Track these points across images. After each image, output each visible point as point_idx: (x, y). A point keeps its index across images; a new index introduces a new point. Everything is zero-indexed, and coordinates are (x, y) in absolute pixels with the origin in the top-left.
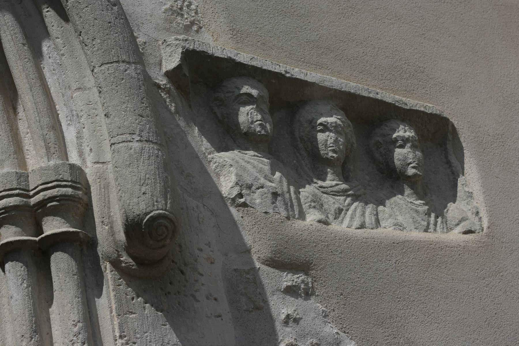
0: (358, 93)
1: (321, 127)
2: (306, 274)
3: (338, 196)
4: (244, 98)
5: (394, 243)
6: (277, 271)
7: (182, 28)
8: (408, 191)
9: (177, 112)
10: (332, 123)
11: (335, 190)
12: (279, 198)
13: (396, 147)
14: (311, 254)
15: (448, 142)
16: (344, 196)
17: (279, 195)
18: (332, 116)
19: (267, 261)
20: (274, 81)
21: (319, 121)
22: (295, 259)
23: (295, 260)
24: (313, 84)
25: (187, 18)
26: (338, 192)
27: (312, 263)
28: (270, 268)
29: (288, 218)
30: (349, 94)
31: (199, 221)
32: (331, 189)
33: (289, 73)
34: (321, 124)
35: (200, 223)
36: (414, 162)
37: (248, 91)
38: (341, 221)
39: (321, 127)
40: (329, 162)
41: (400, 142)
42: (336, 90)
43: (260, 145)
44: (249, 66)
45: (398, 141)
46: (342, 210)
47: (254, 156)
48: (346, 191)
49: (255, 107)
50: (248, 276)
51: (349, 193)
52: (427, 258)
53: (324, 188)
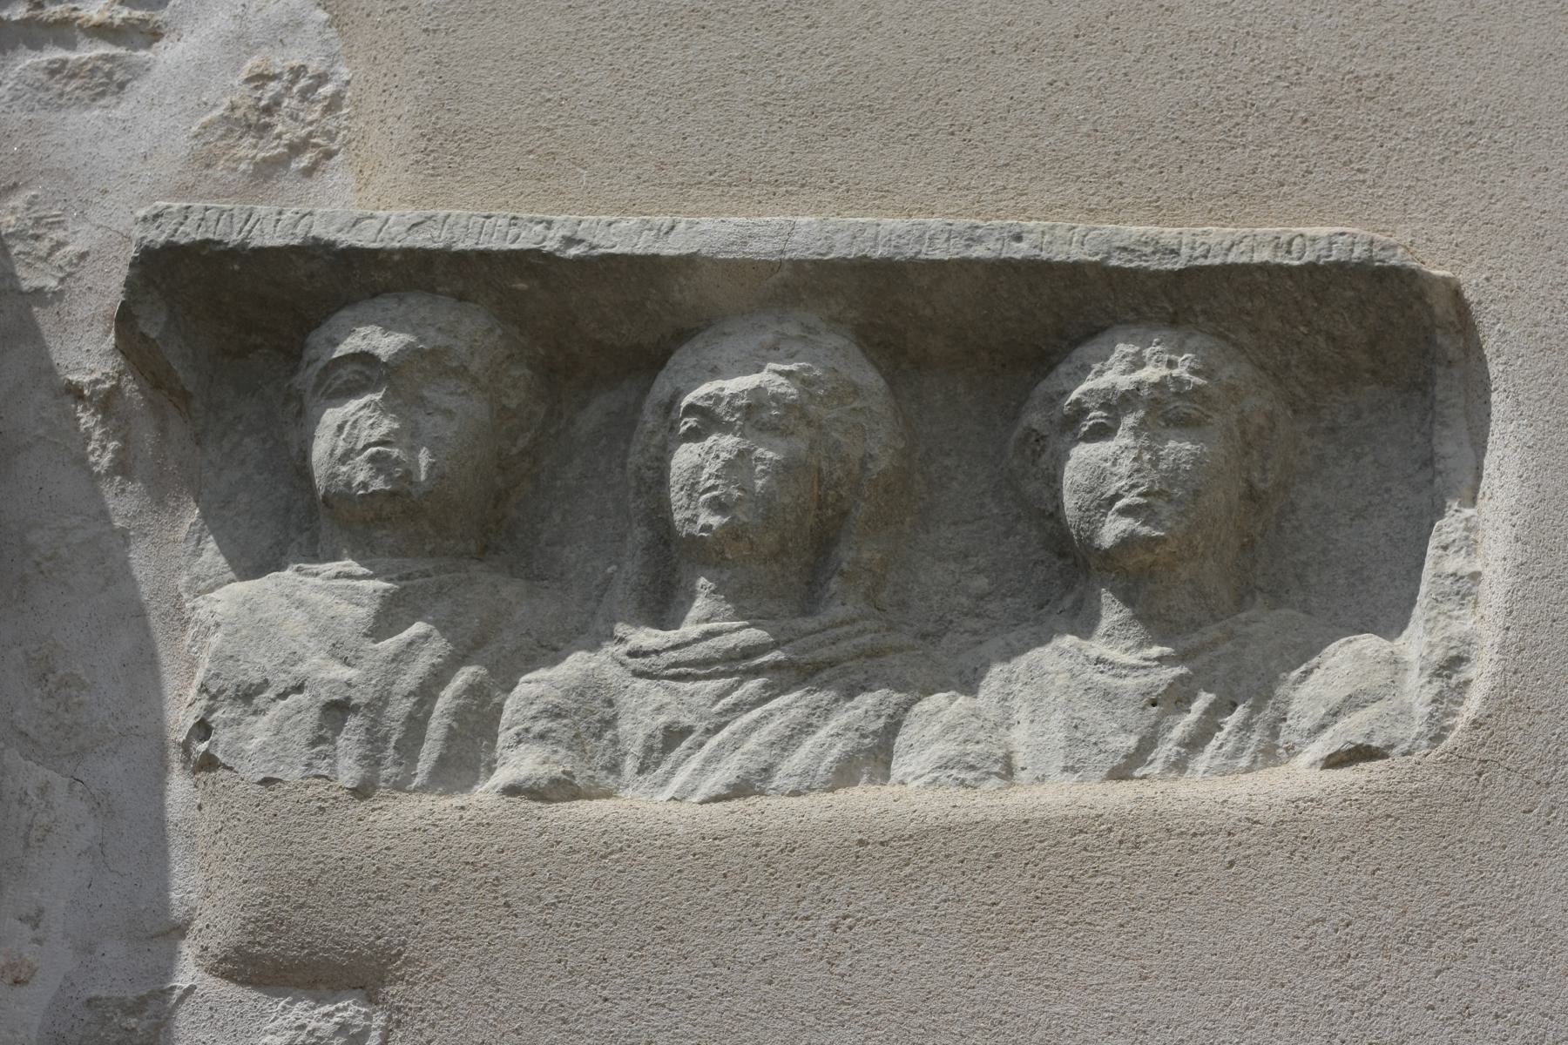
0: (910, 254)
1: (691, 421)
2: (371, 1000)
3: (696, 678)
4: (345, 373)
5: (861, 843)
6: (255, 995)
7: (244, 172)
8: (1112, 613)
9: (122, 467)
10: (734, 396)
11: (692, 657)
12: (353, 721)
13: (1076, 442)
14: (402, 920)
15: (1440, 371)
16: (731, 675)
17: (355, 709)
18: (759, 370)
19: (225, 959)
20: (522, 286)
21: (687, 400)
22: (329, 944)
23: (328, 951)
24: (689, 262)
25: (279, 136)
26: (706, 662)
27: (400, 953)
28: (232, 985)
29: (362, 791)
30: (864, 266)
31: (26, 837)
32: (674, 654)
33: (580, 241)
34: (692, 409)
35: (27, 845)
36: (1133, 486)
37: (364, 346)
38: (659, 780)
39: (691, 421)
40: (704, 553)
41: (1097, 415)
42: (797, 264)
43: (379, 534)
44: (392, 252)
45: (1087, 411)
46: (689, 731)
47: (338, 576)
48: (749, 652)
49: (377, 397)
50: (133, 1022)
51: (758, 661)
52: (1027, 891)
53: (646, 654)
